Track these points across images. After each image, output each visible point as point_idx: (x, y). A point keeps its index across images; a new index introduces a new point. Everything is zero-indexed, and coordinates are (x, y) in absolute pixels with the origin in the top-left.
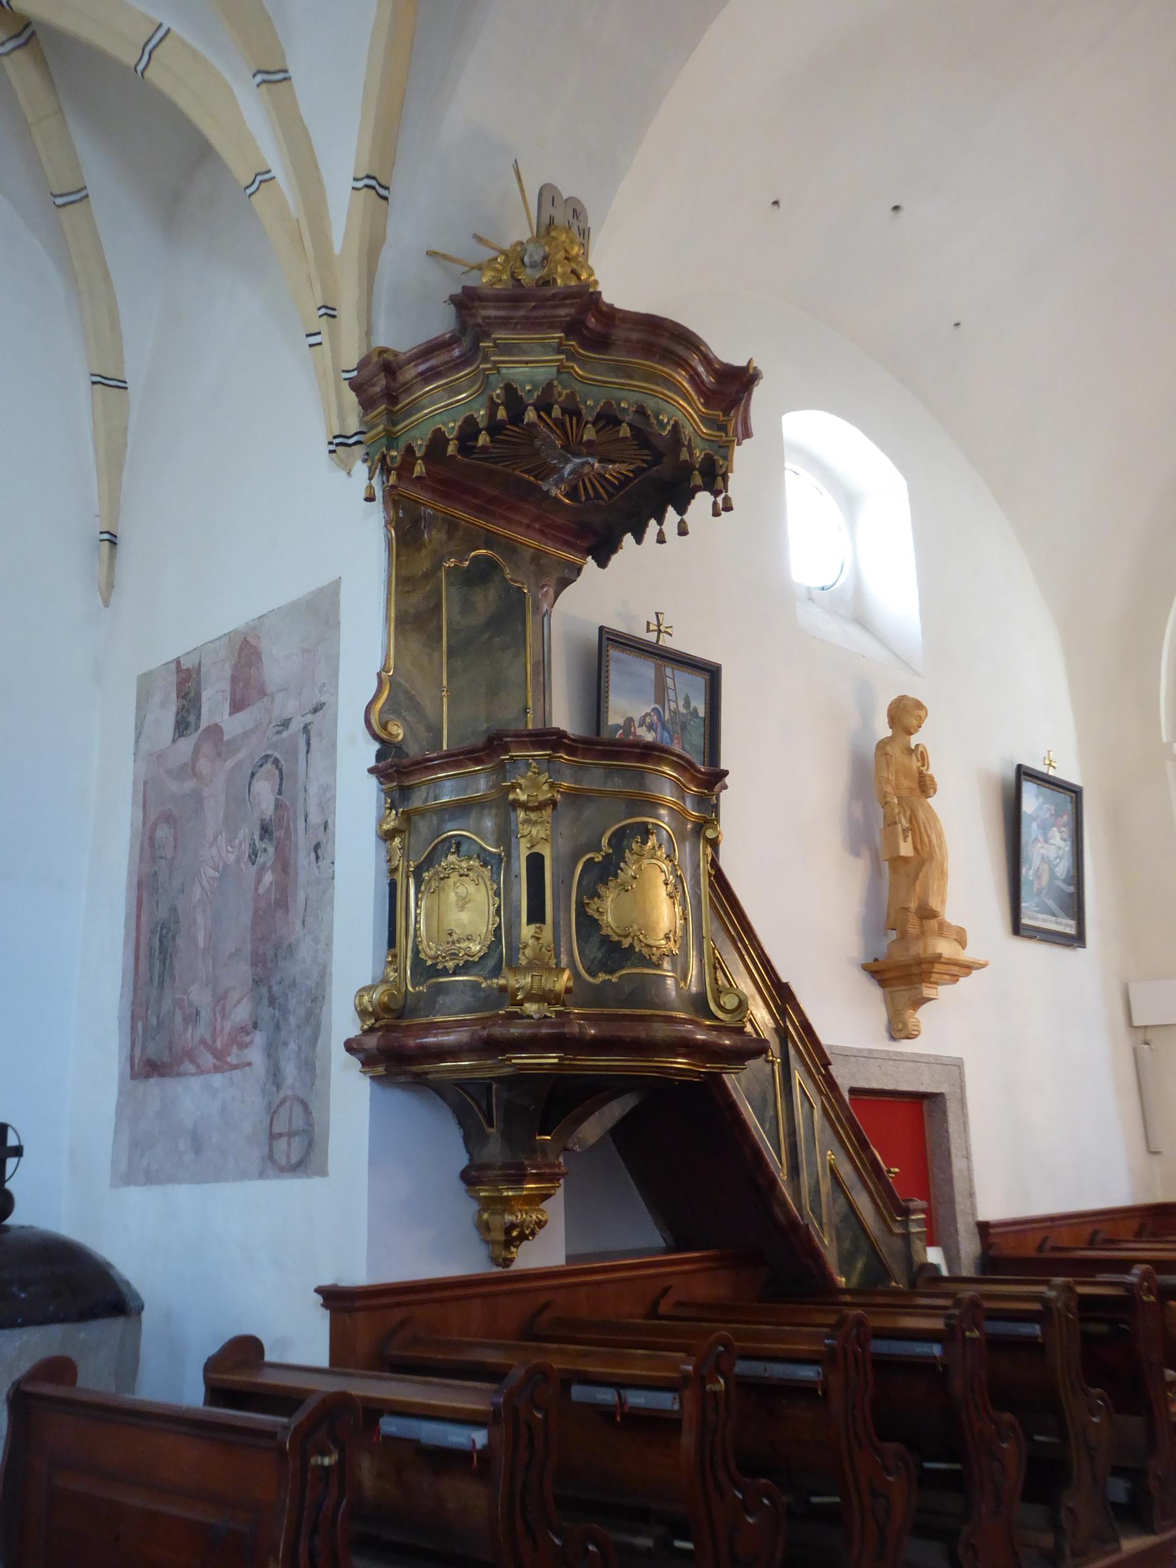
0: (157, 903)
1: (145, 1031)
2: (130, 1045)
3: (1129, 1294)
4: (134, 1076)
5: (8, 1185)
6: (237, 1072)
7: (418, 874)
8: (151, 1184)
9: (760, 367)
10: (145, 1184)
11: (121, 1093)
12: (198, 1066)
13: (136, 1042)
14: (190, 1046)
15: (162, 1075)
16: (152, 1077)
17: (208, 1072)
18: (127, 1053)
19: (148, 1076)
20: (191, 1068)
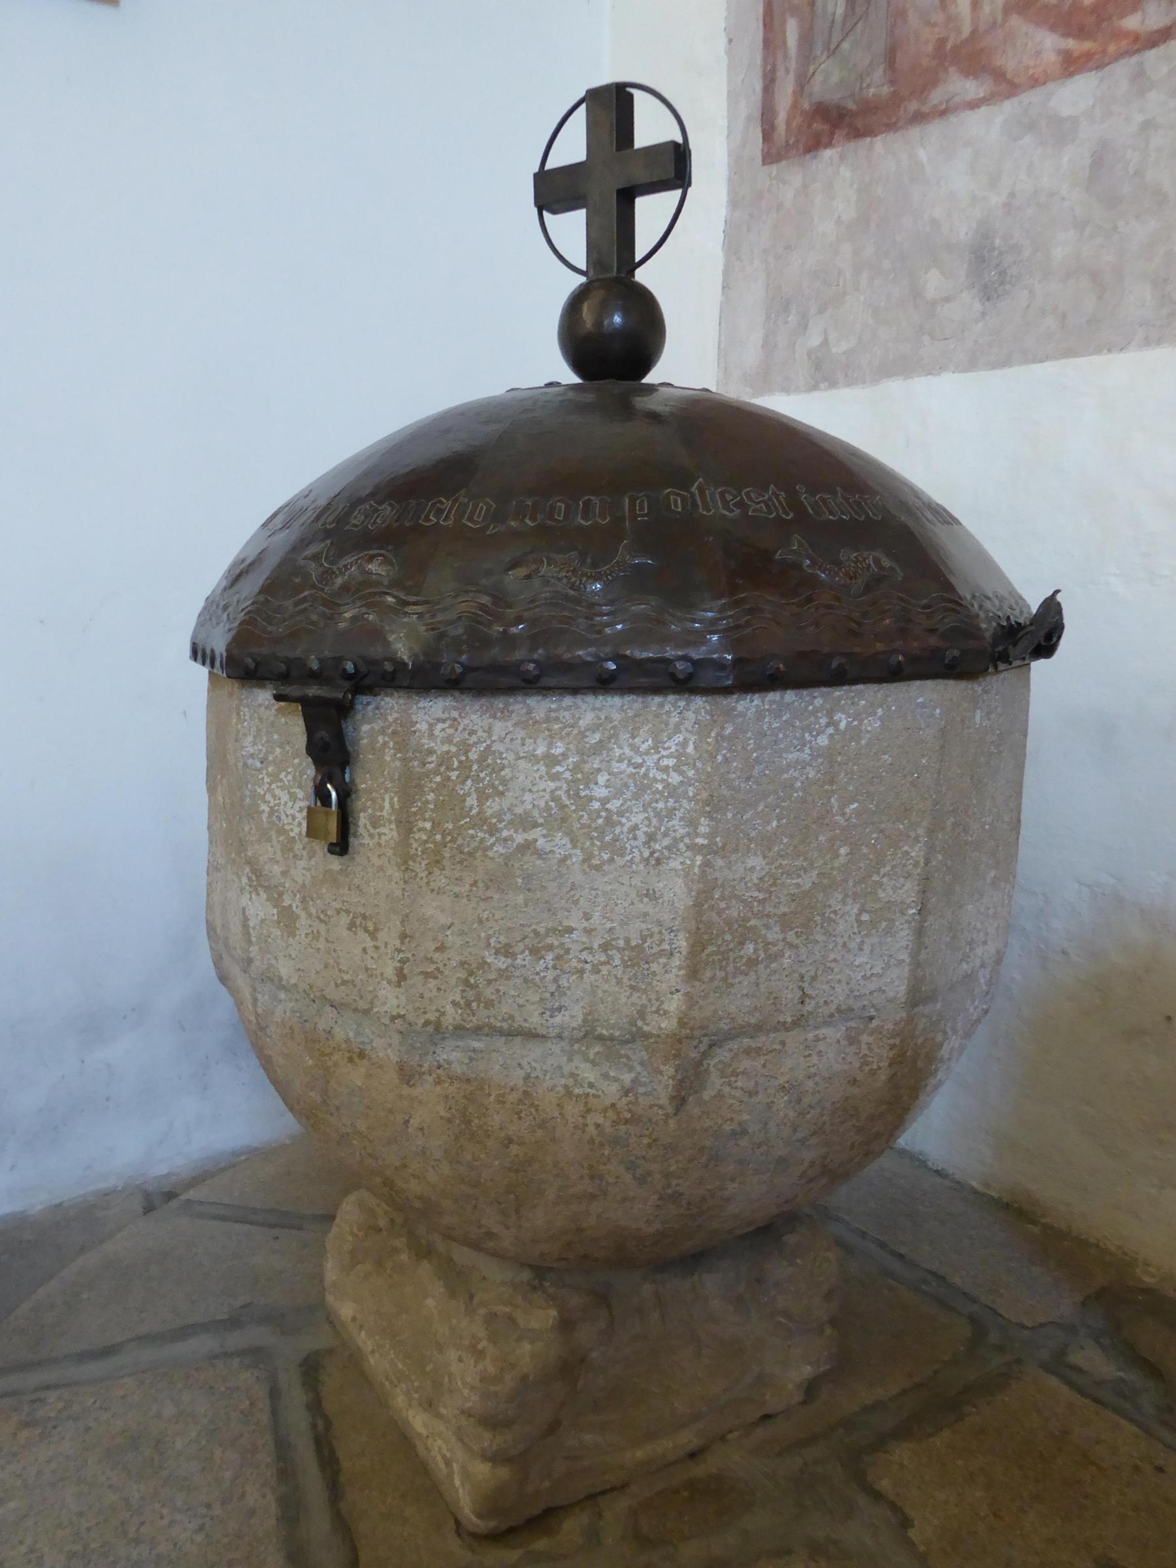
0: (307, 496)
1: (806, 40)
2: (758, 86)
3: (732, 677)
4: (771, 156)
5: (641, 276)
6: (1151, 55)
7: (994, 23)
8: (833, 384)
9: (193, 663)
10: (814, 387)
11: (734, 202)
12: (999, 75)
13: (780, 73)
14: (966, 30)
15: (857, 134)
16: (829, 145)
17: (1035, 82)
18: (751, 104)
19: (815, 145)
20: (971, 88)
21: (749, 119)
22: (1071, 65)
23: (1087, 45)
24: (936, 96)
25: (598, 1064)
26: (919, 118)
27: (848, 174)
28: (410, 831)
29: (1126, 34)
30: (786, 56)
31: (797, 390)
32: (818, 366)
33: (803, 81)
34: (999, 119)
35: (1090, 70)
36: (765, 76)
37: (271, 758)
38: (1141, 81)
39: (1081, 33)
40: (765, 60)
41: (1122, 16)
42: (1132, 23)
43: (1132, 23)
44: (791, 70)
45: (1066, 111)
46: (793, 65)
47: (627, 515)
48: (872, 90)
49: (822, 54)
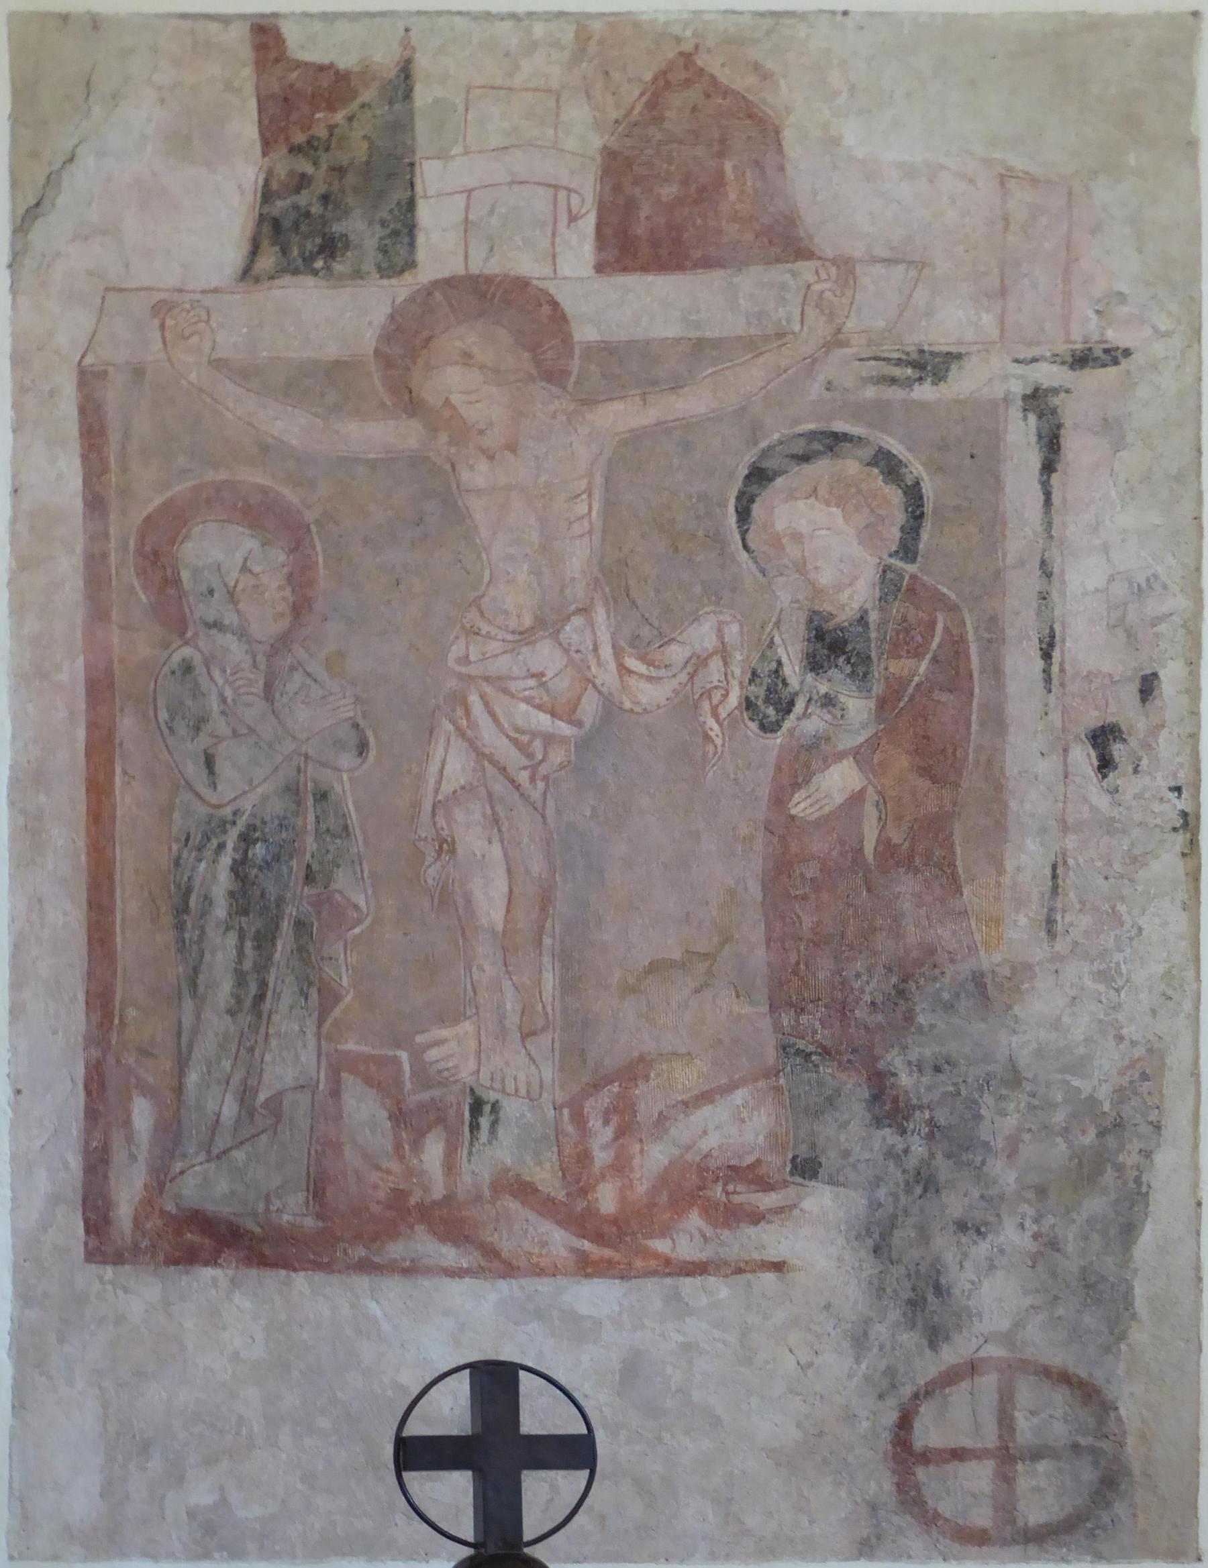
13: (119, 1156)
19: (188, 1258)
20: (449, 1255)
21: (55, 1200)
22: (586, 1267)
23: (608, 1253)
24: (396, 1250)
25: (948, 1335)
26: (366, 1266)
27: (247, 1305)
28: (583, 745)
29: (656, 1255)
30: (129, 1139)
31: (171, 1556)
32: (209, 1529)
33: (160, 1179)
34: (493, 1297)
35: (614, 1277)
36: (87, 1152)
37: (402, 218)
38: (678, 1306)
39: (599, 1238)
40: (88, 1133)
41: (651, 1236)
42: (661, 1246)
43: (661, 1246)
44: (141, 1158)
45: (584, 1309)
46: (143, 1152)
47: (407, 1074)
48: (285, 1217)
49: (197, 1154)
